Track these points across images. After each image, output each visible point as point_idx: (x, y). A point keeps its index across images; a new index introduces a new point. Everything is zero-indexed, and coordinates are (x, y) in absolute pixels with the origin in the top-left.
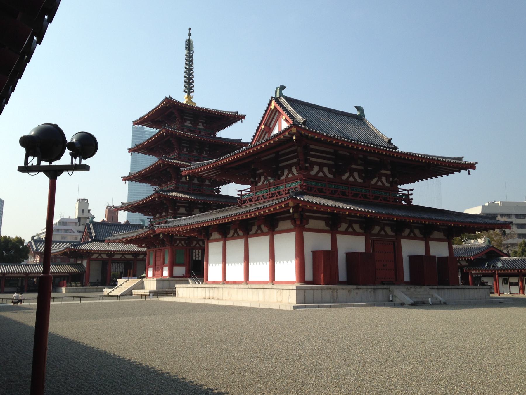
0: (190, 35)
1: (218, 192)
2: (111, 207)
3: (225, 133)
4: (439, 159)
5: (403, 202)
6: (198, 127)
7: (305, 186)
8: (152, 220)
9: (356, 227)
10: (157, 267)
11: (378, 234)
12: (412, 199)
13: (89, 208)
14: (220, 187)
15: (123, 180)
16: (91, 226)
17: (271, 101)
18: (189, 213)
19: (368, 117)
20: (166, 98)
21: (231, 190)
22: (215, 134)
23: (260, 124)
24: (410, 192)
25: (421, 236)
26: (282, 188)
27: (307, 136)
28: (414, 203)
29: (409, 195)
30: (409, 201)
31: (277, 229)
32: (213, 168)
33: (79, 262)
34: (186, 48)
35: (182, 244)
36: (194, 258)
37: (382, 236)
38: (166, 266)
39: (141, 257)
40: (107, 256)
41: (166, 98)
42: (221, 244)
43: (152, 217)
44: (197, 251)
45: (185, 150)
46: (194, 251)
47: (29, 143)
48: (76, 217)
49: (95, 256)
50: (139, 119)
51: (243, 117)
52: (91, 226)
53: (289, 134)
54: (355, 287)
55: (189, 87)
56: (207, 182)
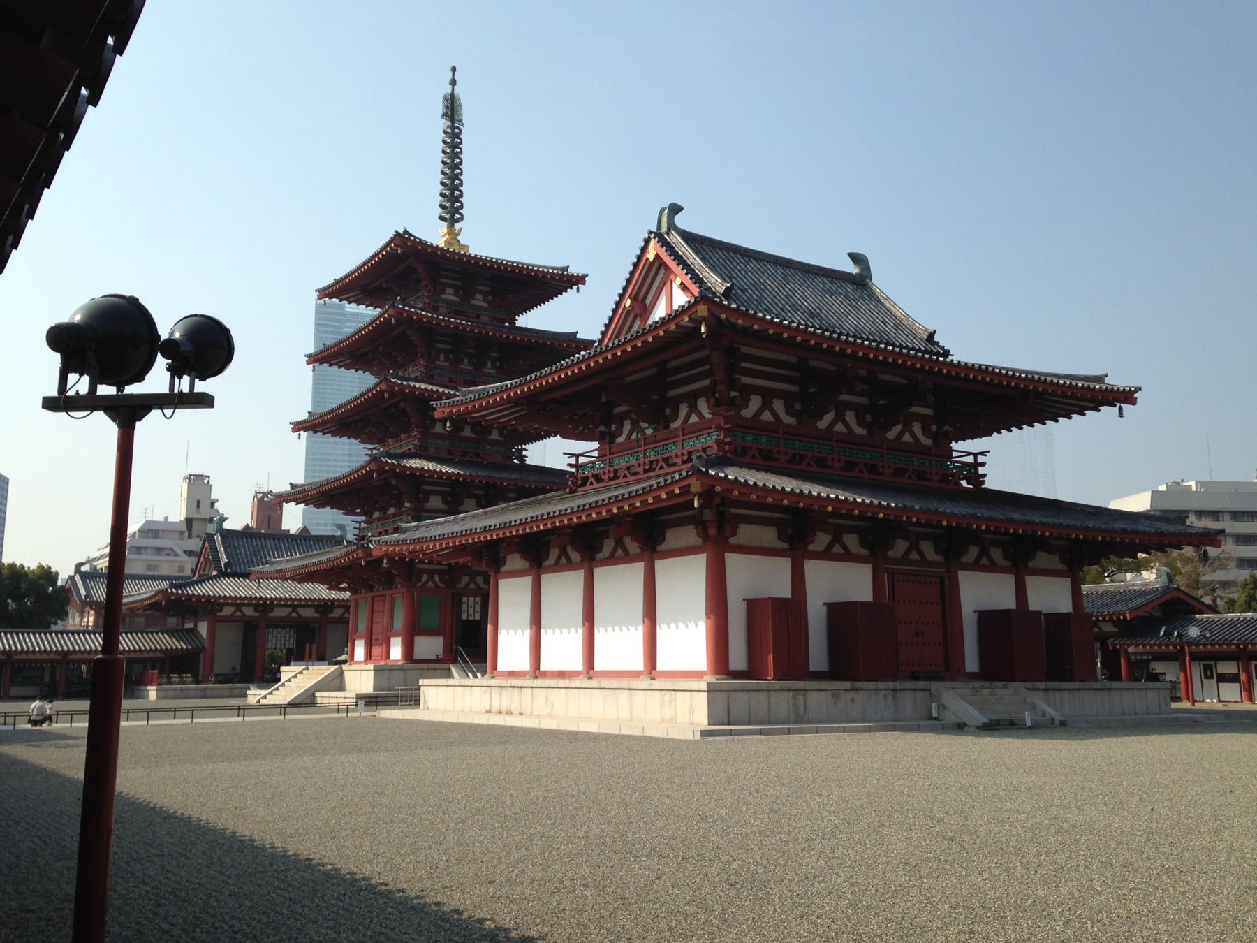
0: (453, 82)
1: (522, 458)
2: (265, 495)
3: (539, 319)
4: (1049, 379)
5: (964, 483)
6: (474, 302)
7: (729, 443)
8: (363, 525)
9: (852, 541)
10: (374, 637)
11: (904, 559)
12: (984, 476)
13: (213, 496)
14: (527, 447)
15: (294, 431)
16: (218, 538)
17: (647, 242)
18: (453, 508)
19: (881, 280)
20: (397, 234)
21: (552, 453)
22: (513, 321)
23: (622, 296)
24: (980, 459)
25: (1006, 563)
26: (674, 449)
27: (735, 325)
28: (990, 484)
29: (977, 465)
30: (977, 480)
31: (661, 548)
32: (509, 402)
33: (189, 625)
34: (445, 115)
35: (434, 582)
36: (464, 617)
37: (913, 562)
38: (396, 635)
39: (337, 613)
40: (256, 611)
41: (397, 234)
42: (527, 582)
43: (363, 518)
44: (471, 599)
45: (442, 358)
46: (465, 599)
47: (69, 342)
48: (183, 518)
49: (227, 611)
50: (333, 285)
51: (580, 280)
52: (218, 538)
53: (691, 320)
54: (847, 685)
55: (452, 208)
56: (495, 435)
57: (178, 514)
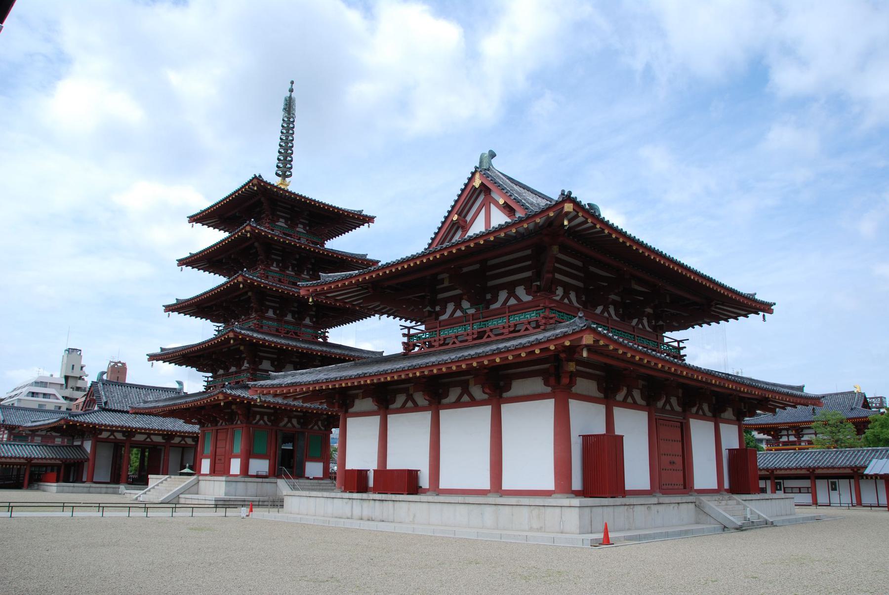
0: (291, 90)
1: (325, 338)
2: (116, 363)
6: (298, 229)
13: (83, 363)
15: (149, 360)
17: (473, 174)
22: (323, 244)
23: (450, 212)
24: (681, 345)
26: (493, 323)
28: (329, 340)
29: (679, 349)
31: (351, 410)
33: (77, 443)
34: (285, 109)
35: (462, 310)
40: (163, 438)
42: (376, 419)
43: (211, 374)
45: (275, 265)
49: (105, 435)
55: (285, 166)
57: (58, 376)
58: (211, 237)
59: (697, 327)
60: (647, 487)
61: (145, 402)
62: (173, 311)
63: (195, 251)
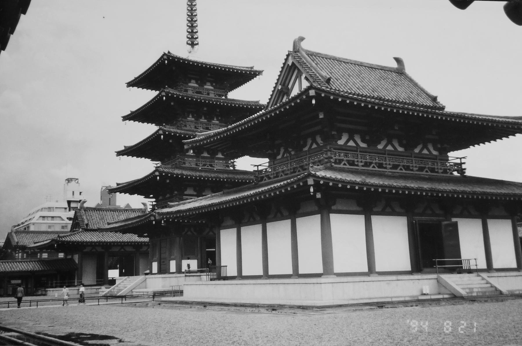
1: (234, 166)
3: (240, 94)
12: (465, 169)
14: (235, 160)
17: (288, 56)
18: (199, 194)
21: (246, 163)
23: (276, 84)
24: (463, 161)
30: (462, 171)
35: (191, 232)
39: (144, 249)
43: (154, 200)
49: (87, 250)
51: (259, 73)
55: (192, 42)
58: (147, 95)
59: (471, 147)
60: (409, 268)
61: (109, 224)
62: (123, 155)
63: (134, 109)
